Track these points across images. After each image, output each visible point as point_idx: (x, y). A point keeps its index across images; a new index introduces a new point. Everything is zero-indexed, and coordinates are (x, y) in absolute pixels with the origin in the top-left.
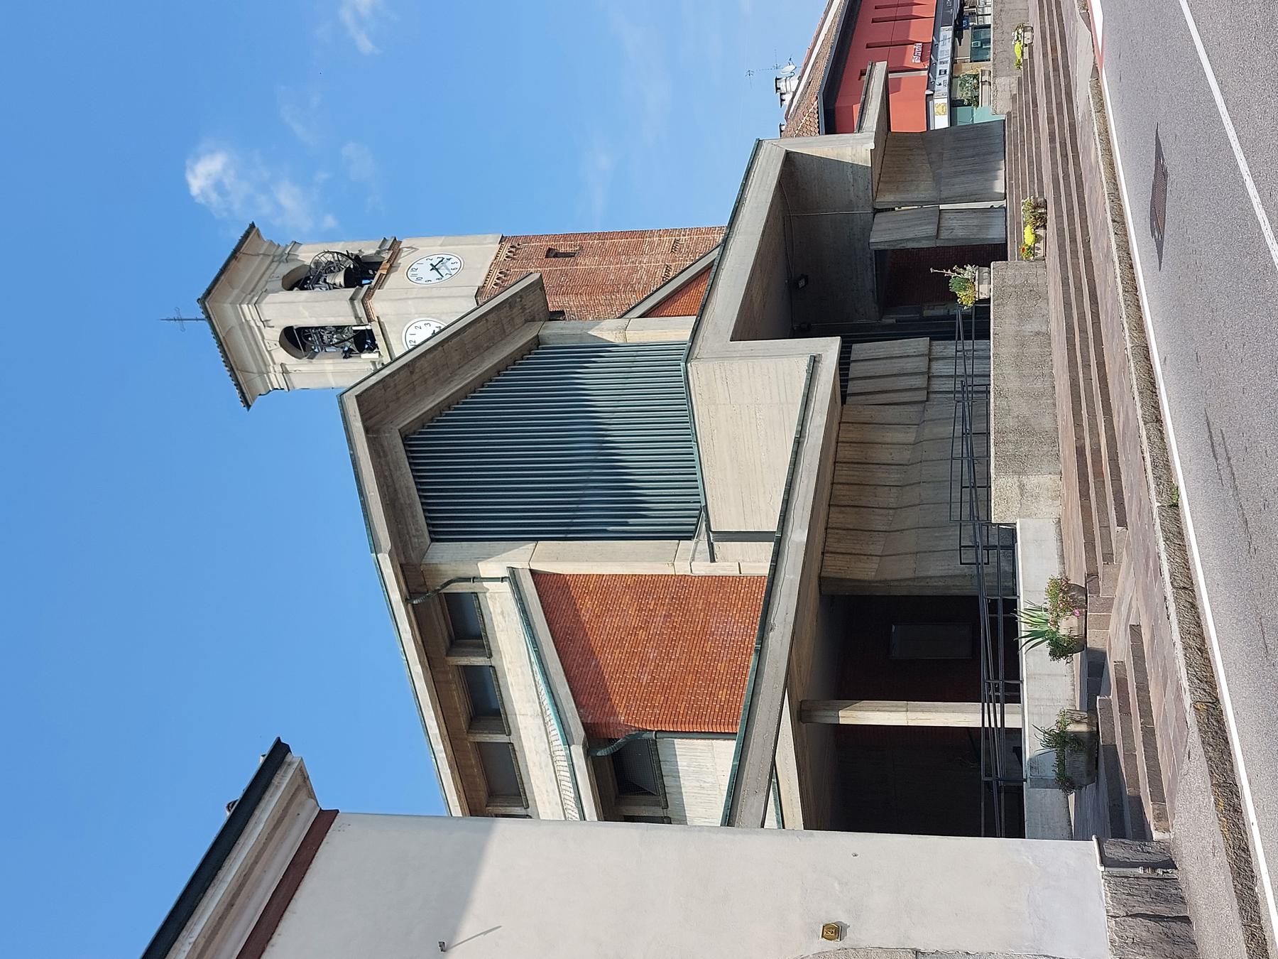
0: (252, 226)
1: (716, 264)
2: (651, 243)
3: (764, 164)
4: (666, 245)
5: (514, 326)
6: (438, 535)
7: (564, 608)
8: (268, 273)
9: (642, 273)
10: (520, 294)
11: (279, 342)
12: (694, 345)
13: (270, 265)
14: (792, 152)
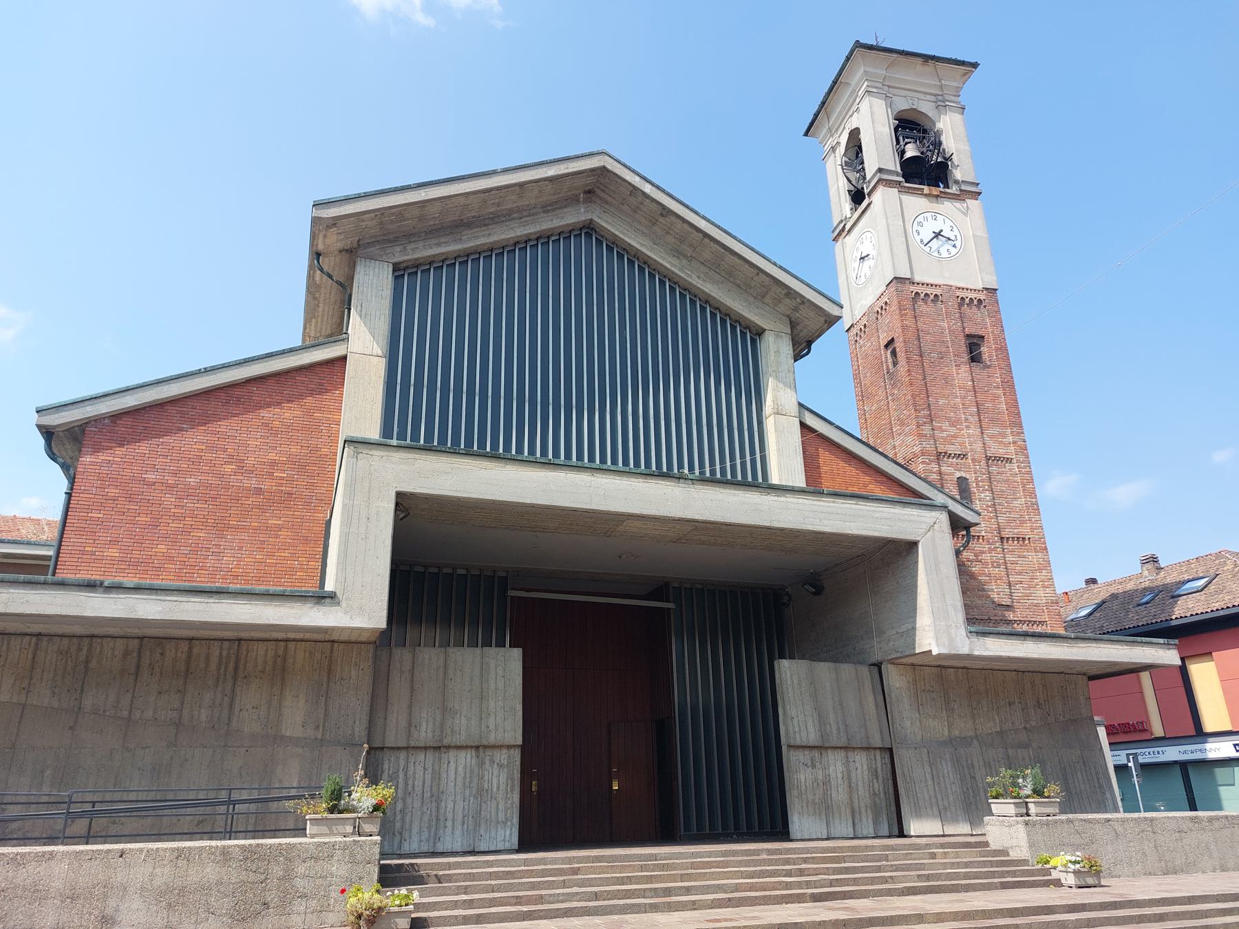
0: (975, 65)
1: (927, 502)
2: (1004, 435)
3: (877, 515)
4: (1001, 450)
5: (776, 306)
6: (399, 271)
7: (285, 392)
8: (920, 95)
9: (953, 431)
10: (805, 301)
11: (851, 131)
12: (395, 449)
13: (931, 94)
14: (918, 548)
